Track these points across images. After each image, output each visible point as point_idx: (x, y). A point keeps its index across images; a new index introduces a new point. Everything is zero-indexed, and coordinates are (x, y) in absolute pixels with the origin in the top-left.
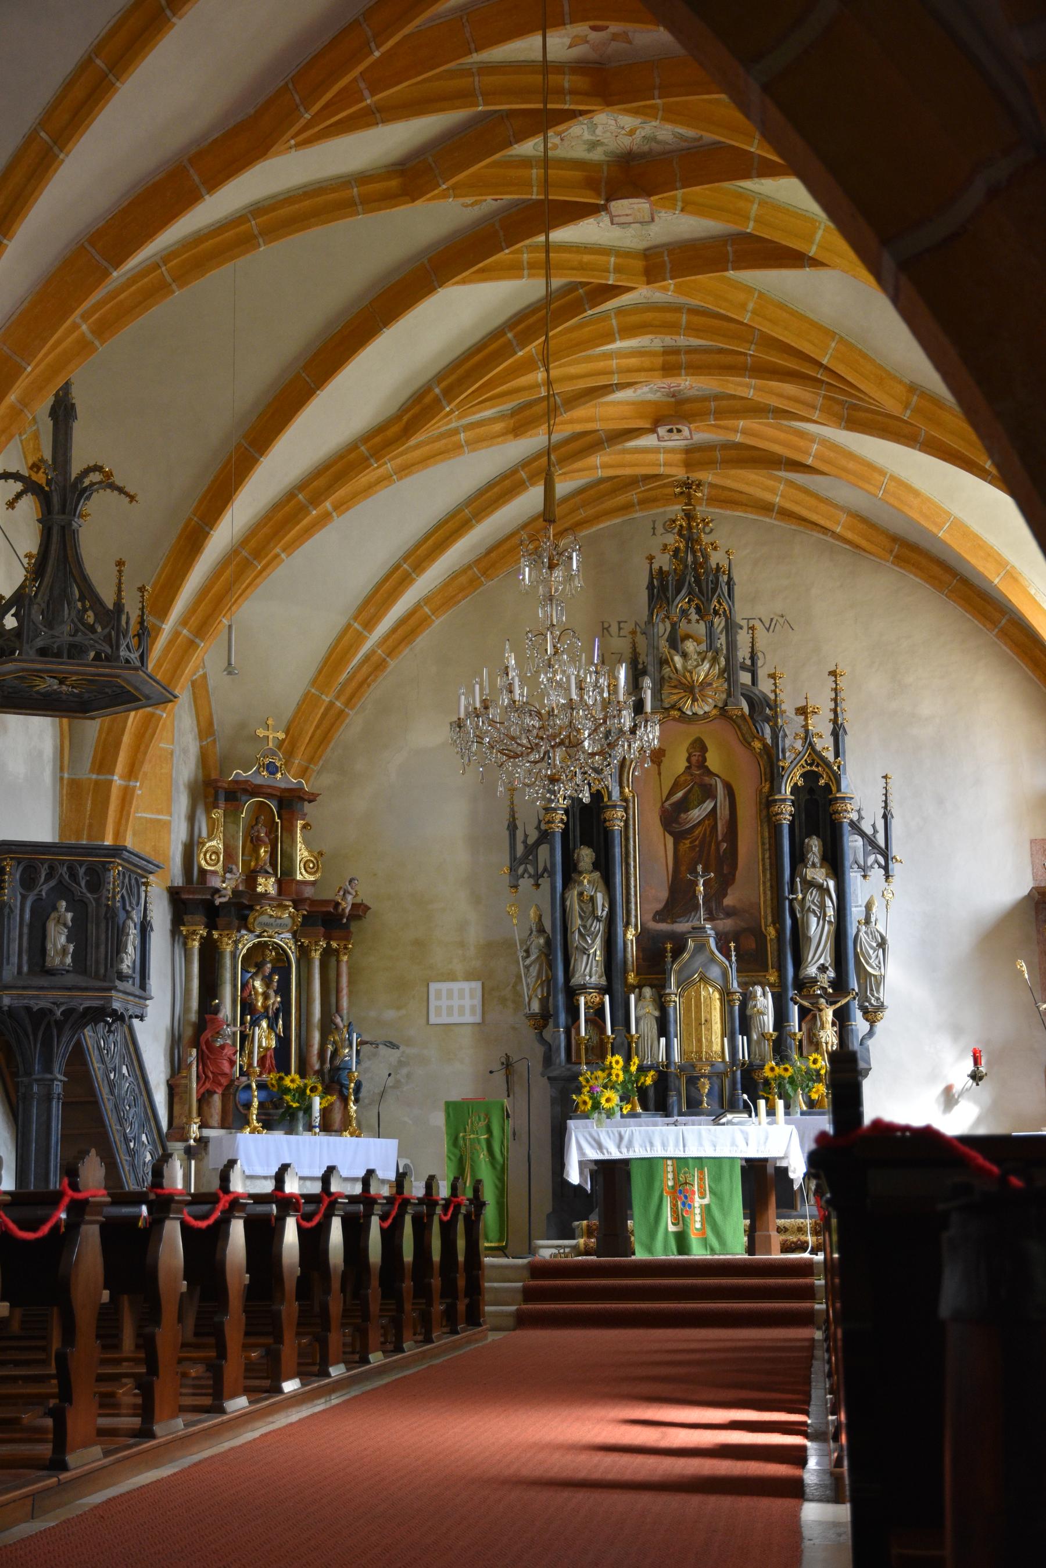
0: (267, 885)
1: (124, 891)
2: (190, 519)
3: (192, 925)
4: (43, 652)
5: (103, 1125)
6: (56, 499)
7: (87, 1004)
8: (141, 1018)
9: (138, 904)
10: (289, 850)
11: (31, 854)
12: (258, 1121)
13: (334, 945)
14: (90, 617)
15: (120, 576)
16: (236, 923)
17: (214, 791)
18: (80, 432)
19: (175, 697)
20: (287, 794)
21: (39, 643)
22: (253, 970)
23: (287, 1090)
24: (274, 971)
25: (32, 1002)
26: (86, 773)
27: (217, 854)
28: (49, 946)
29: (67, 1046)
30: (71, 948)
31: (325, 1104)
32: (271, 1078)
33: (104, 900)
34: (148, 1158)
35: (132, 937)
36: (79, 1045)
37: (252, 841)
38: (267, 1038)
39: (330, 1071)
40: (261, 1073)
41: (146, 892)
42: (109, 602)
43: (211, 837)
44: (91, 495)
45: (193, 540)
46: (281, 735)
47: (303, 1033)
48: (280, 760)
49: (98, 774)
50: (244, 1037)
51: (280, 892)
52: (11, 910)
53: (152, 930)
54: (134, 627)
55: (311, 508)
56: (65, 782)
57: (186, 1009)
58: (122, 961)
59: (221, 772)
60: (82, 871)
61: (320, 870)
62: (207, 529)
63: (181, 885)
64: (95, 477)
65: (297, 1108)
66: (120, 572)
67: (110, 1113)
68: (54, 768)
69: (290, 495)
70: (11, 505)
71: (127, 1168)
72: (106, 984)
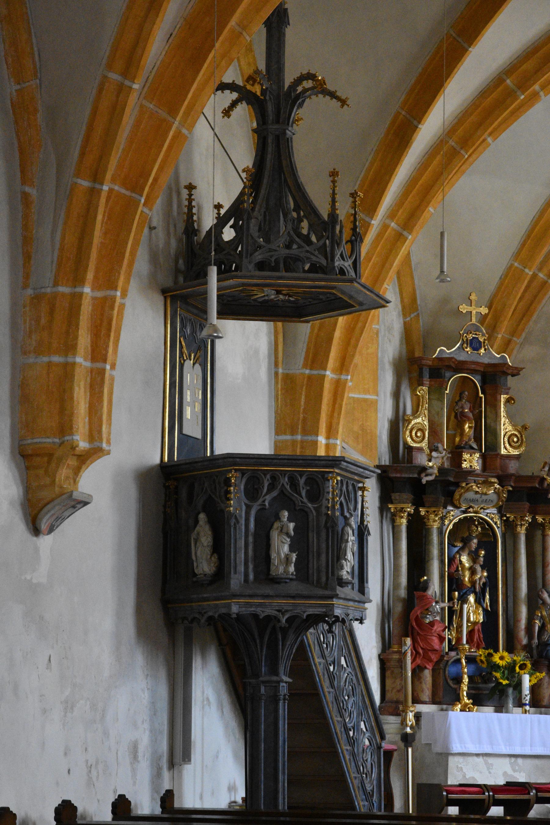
0: (472, 461)
1: (342, 498)
2: (398, 114)
3: (400, 503)
4: (261, 266)
5: (325, 717)
6: (270, 108)
7: (311, 611)
8: (361, 621)
9: (355, 508)
10: (492, 424)
11: (254, 465)
12: (469, 696)
13: (540, 519)
14: (305, 226)
15: (334, 187)
16: (442, 499)
17: (417, 368)
18: (291, 35)
19: (388, 302)
20: (490, 370)
21: (258, 257)
22: (460, 545)
23: (496, 667)
24: (480, 546)
25: (259, 610)
26: (299, 369)
27: (422, 431)
28: (273, 555)
29: (292, 649)
30: (294, 557)
31: (534, 681)
32: (481, 653)
33: (324, 510)
34: (367, 743)
35: (350, 543)
36: (302, 641)
37: (456, 417)
38: (474, 613)
39: (537, 646)
40: (470, 649)
41: (363, 496)
42: (325, 214)
43: (416, 412)
44: (303, 101)
45: (401, 135)
46: (484, 310)
47: (511, 604)
48: (483, 335)
49: (311, 369)
50: (451, 612)
51: (485, 468)
52: (237, 521)
53: (369, 534)
54: (347, 235)
55: (519, 93)
56: (280, 377)
57: (396, 585)
58: (342, 568)
59: (425, 346)
60: (302, 481)
61: (524, 444)
62: (415, 123)
63: (387, 464)
64: (308, 84)
65: (507, 685)
66: (334, 182)
67: (330, 705)
68: (269, 363)
69: (498, 80)
70: (227, 113)
71: (347, 757)
72: (327, 593)
